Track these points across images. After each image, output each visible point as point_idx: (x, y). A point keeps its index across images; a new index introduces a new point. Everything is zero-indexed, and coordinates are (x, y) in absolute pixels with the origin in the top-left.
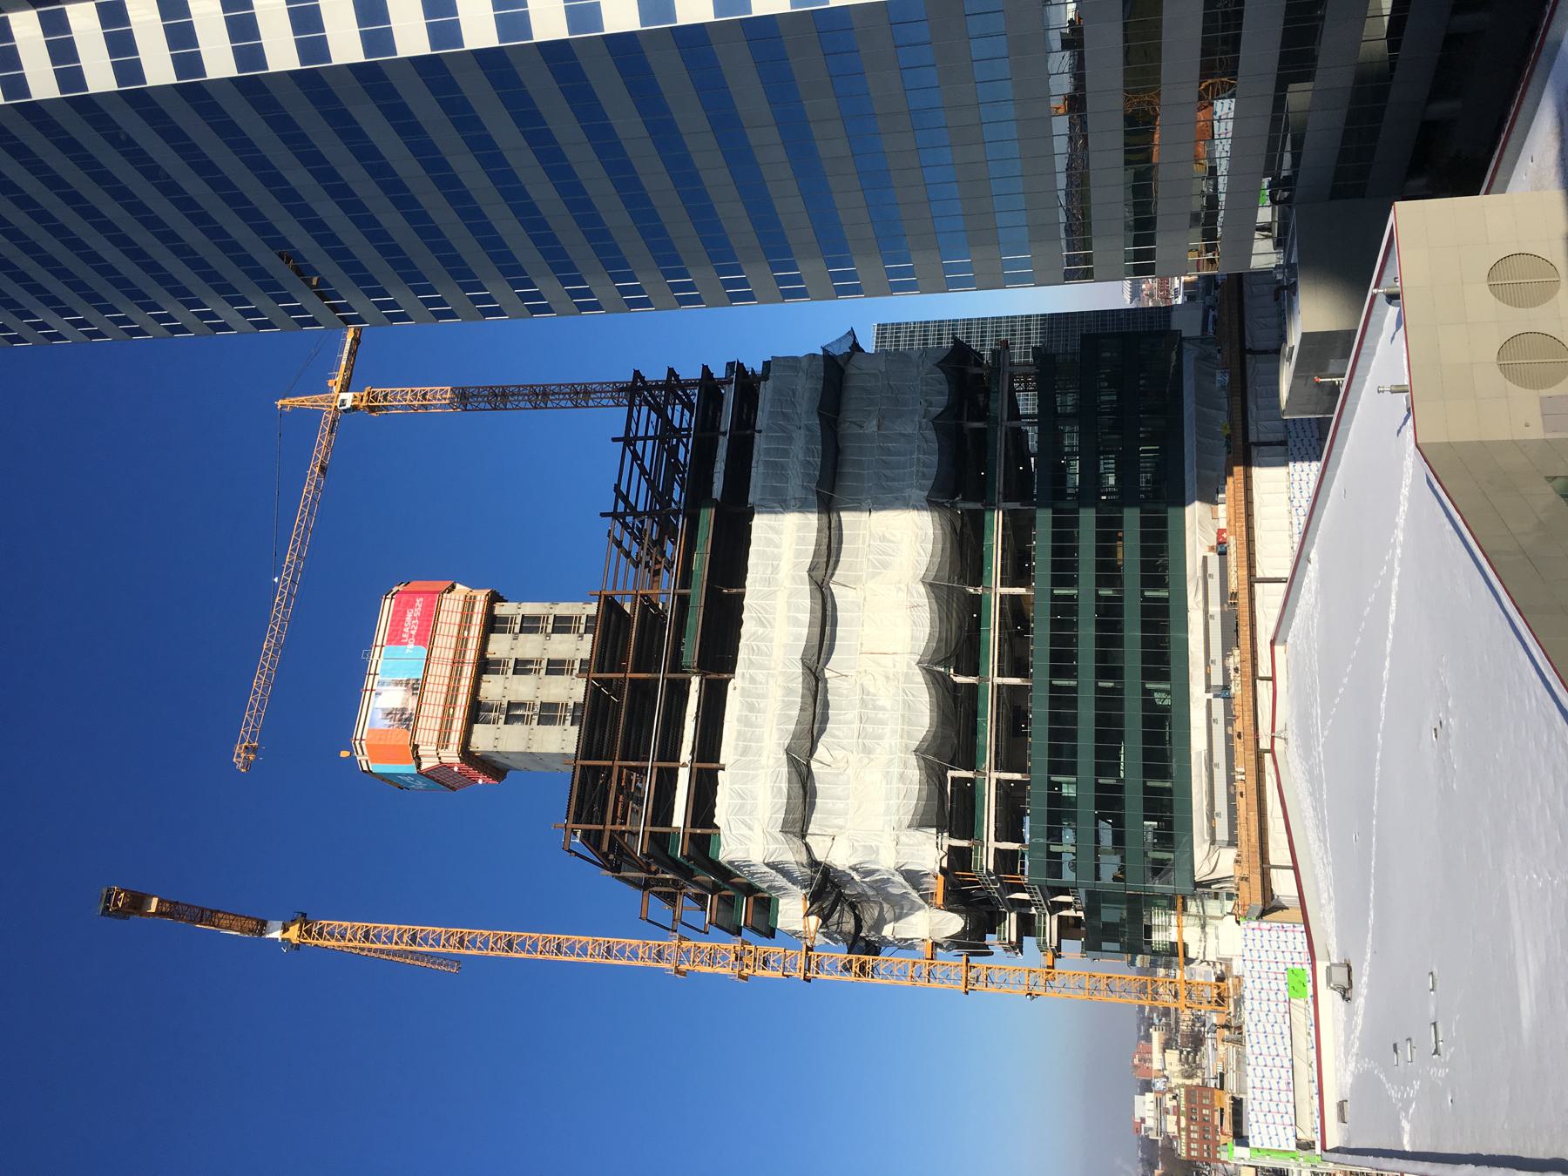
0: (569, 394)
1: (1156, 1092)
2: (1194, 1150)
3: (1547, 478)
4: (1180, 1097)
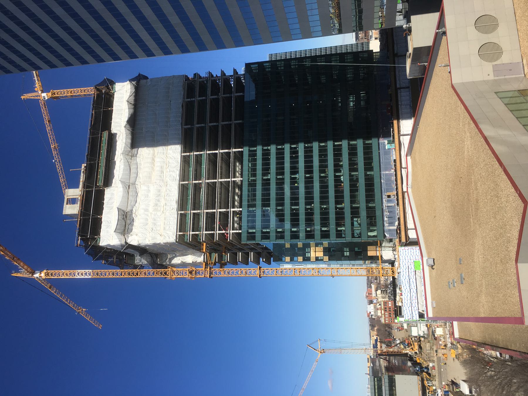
2: (387, 320)
3: (495, 92)
4: (382, 304)
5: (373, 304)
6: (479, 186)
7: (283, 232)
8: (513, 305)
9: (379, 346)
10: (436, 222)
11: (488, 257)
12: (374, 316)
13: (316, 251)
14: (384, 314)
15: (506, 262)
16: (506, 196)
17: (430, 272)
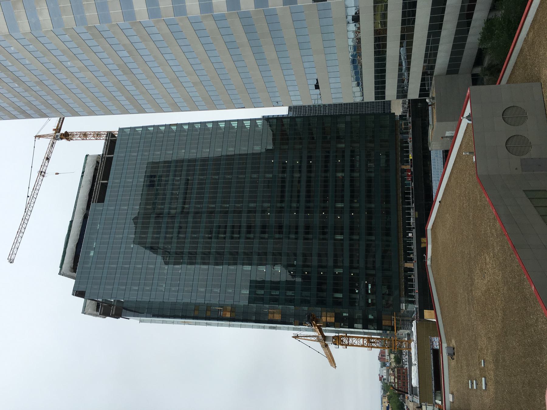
0: (487, 304)
1: (387, 367)
5: (385, 367)
7: (306, 212)
12: (387, 380)
14: (398, 382)
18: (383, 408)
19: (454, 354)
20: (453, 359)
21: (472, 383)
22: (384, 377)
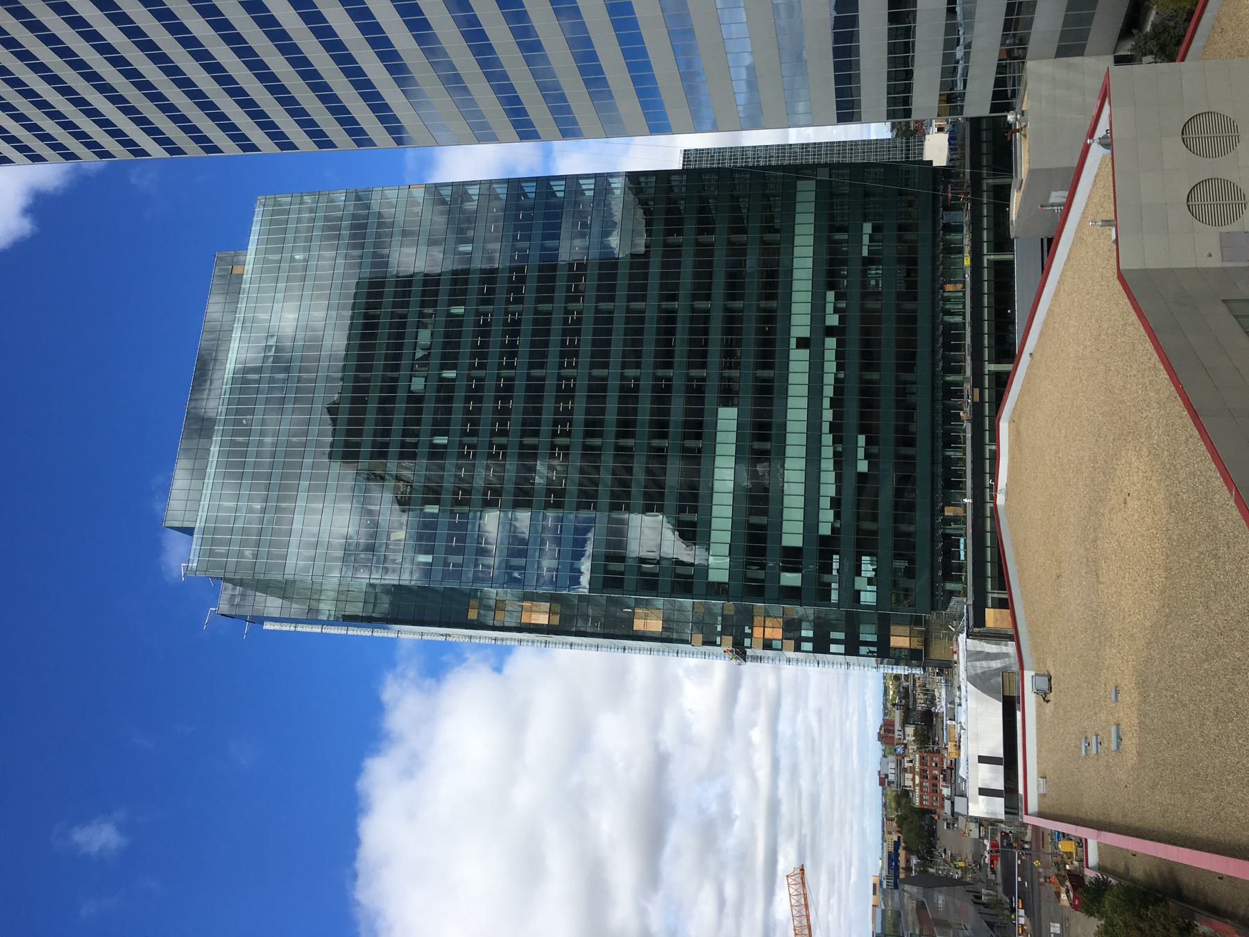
2: (926, 800)
3: (1223, 300)
4: (915, 761)
6: (1171, 523)
8: (1237, 825)
9: (902, 858)
10: (1061, 590)
11: (1184, 697)
13: (766, 625)
14: (921, 783)
15: (1228, 719)
16: (1236, 558)
17: (1039, 706)
18: (885, 844)
19: (1050, 689)
20: (1048, 701)
21: (1089, 744)
22: (889, 778)
